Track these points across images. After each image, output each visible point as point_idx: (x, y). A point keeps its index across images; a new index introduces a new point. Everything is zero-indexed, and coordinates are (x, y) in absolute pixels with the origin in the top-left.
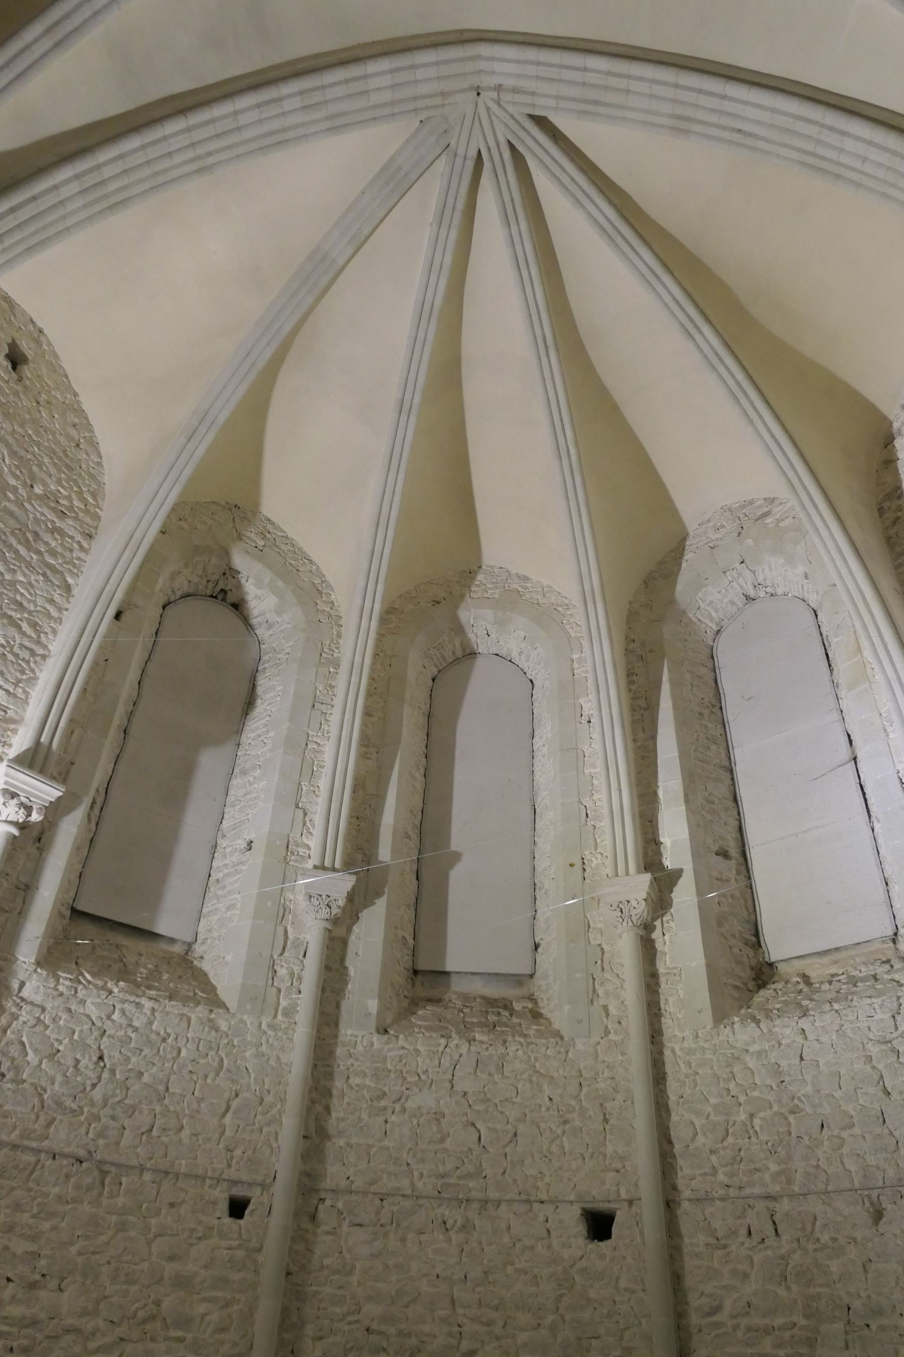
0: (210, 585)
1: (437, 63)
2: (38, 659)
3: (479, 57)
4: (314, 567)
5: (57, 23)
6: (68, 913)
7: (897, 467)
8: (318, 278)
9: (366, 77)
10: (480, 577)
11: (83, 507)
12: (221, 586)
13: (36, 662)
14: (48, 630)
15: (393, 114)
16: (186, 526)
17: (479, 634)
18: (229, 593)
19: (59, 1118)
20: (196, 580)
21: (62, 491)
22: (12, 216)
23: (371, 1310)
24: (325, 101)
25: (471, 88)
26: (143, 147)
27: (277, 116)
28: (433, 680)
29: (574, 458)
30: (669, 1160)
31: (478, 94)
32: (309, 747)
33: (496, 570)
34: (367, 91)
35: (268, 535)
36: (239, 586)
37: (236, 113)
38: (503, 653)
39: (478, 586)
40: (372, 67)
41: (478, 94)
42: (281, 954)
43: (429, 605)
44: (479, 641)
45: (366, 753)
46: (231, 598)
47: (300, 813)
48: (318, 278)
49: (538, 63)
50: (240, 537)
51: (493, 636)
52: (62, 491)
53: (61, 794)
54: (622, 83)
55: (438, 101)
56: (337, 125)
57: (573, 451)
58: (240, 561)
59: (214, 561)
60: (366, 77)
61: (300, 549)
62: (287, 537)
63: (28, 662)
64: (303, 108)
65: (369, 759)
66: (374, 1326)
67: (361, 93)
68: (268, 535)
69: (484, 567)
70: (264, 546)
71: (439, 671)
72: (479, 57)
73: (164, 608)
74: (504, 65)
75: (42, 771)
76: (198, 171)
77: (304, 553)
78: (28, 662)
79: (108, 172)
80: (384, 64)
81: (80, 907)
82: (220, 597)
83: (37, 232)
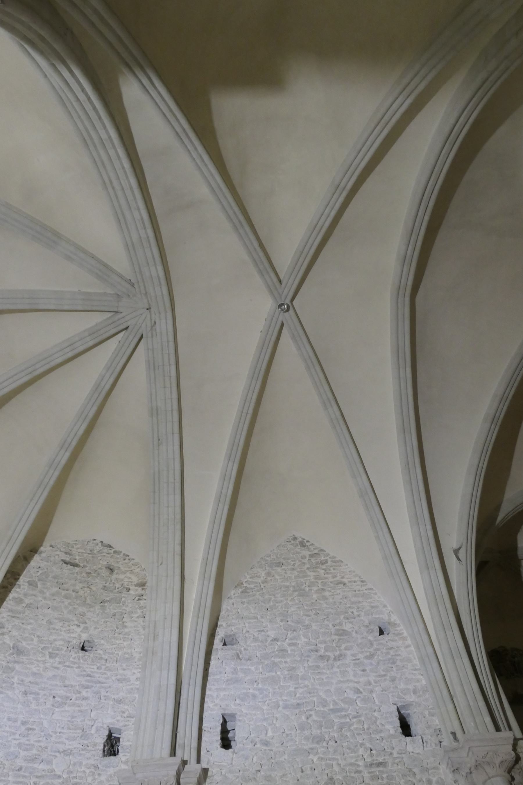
1: (162, 295)
3: (166, 312)
5: (187, 135)
7: (34, 556)
8: (48, 236)
9: (155, 265)
11: (256, 620)
15: (135, 272)
19: (36, 732)
22: (91, 108)
25: (149, 305)
26: (123, 168)
27: (137, 226)
31: (148, 309)
34: (149, 266)
37: (138, 209)
40: (160, 268)
41: (148, 309)
48: (48, 236)
49: (168, 342)
54: (168, 385)
55: (143, 292)
56: (129, 247)
60: (155, 265)
64: (140, 238)
72: (166, 312)
74: (164, 325)
76: (104, 183)
79: (112, 152)
80: (161, 273)
83: (79, 117)
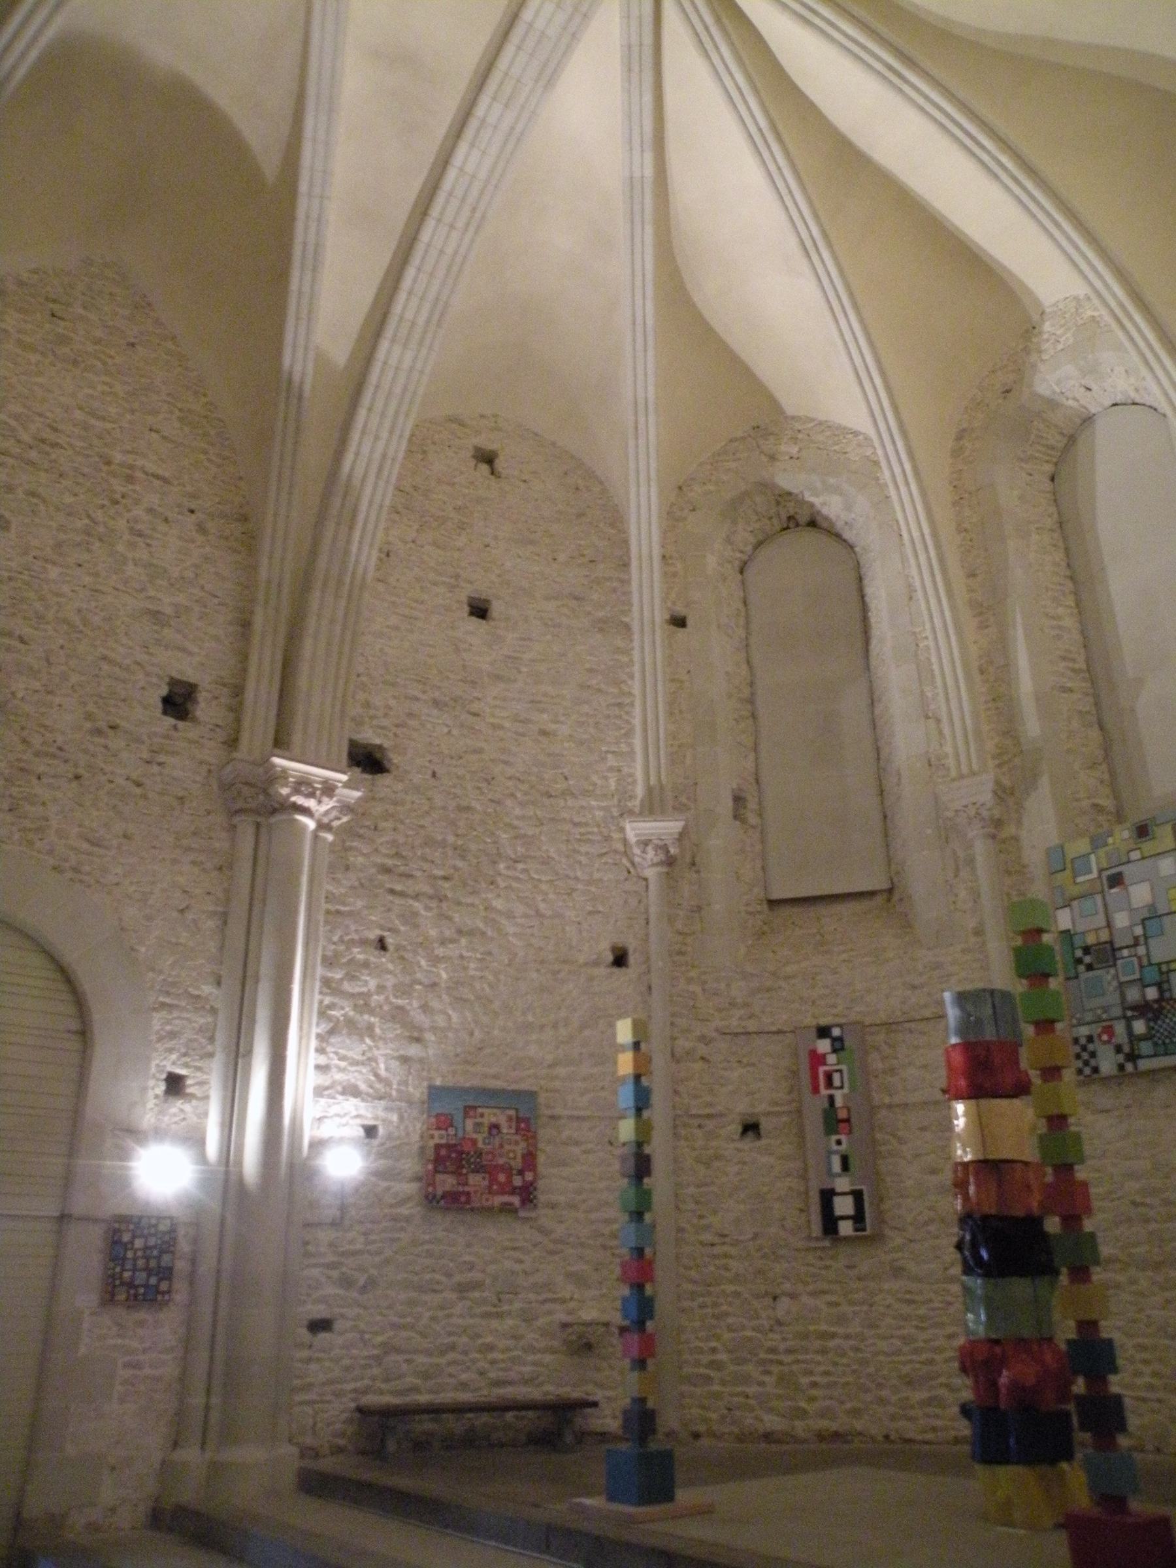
0: (775, 521)
2: (626, 709)
4: (861, 437)
6: (765, 906)
10: (1047, 327)
12: (784, 517)
13: (627, 713)
14: (625, 677)
16: (712, 488)
17: (1077, 396)
18: (797, 517)
20: (757, 526)
21: (582, 542)
23: (1132, 1186)
24: (518, 81)
28: (1053, 479)
29: (1010, 165)
30: (1150, 1015)
32: (921, 645)
33: (1061, 306)
35: (800, 436)
36: (801, 502)
38: (1118, 399)
39: (1048, 340)
42: (956, 876)
43: (1000, 401)
44: (1082, 402)
45: (982, 622)
46: (803, 519)
47: (932, 724)
50: (772, 458)
51: (1094, 387)
52: (582, 542)
53: (683, 823)
57: (1004, 159)
58: (786, 480)
59: (758, 499)
61: (839, 427)
62: (820, 423)
63: (620, 717)
65: (987, 627)
66: (1138, 1199)
67: (539, 42)
68: (800, 436)
69: (1048, 310)
70: (800, 450)
71: (1056, 464)
73: (741, 572)
75: (663, 812)
77: (845, 428)
78: (620, 717)
81: (776, 896)
82: (792, 525)
